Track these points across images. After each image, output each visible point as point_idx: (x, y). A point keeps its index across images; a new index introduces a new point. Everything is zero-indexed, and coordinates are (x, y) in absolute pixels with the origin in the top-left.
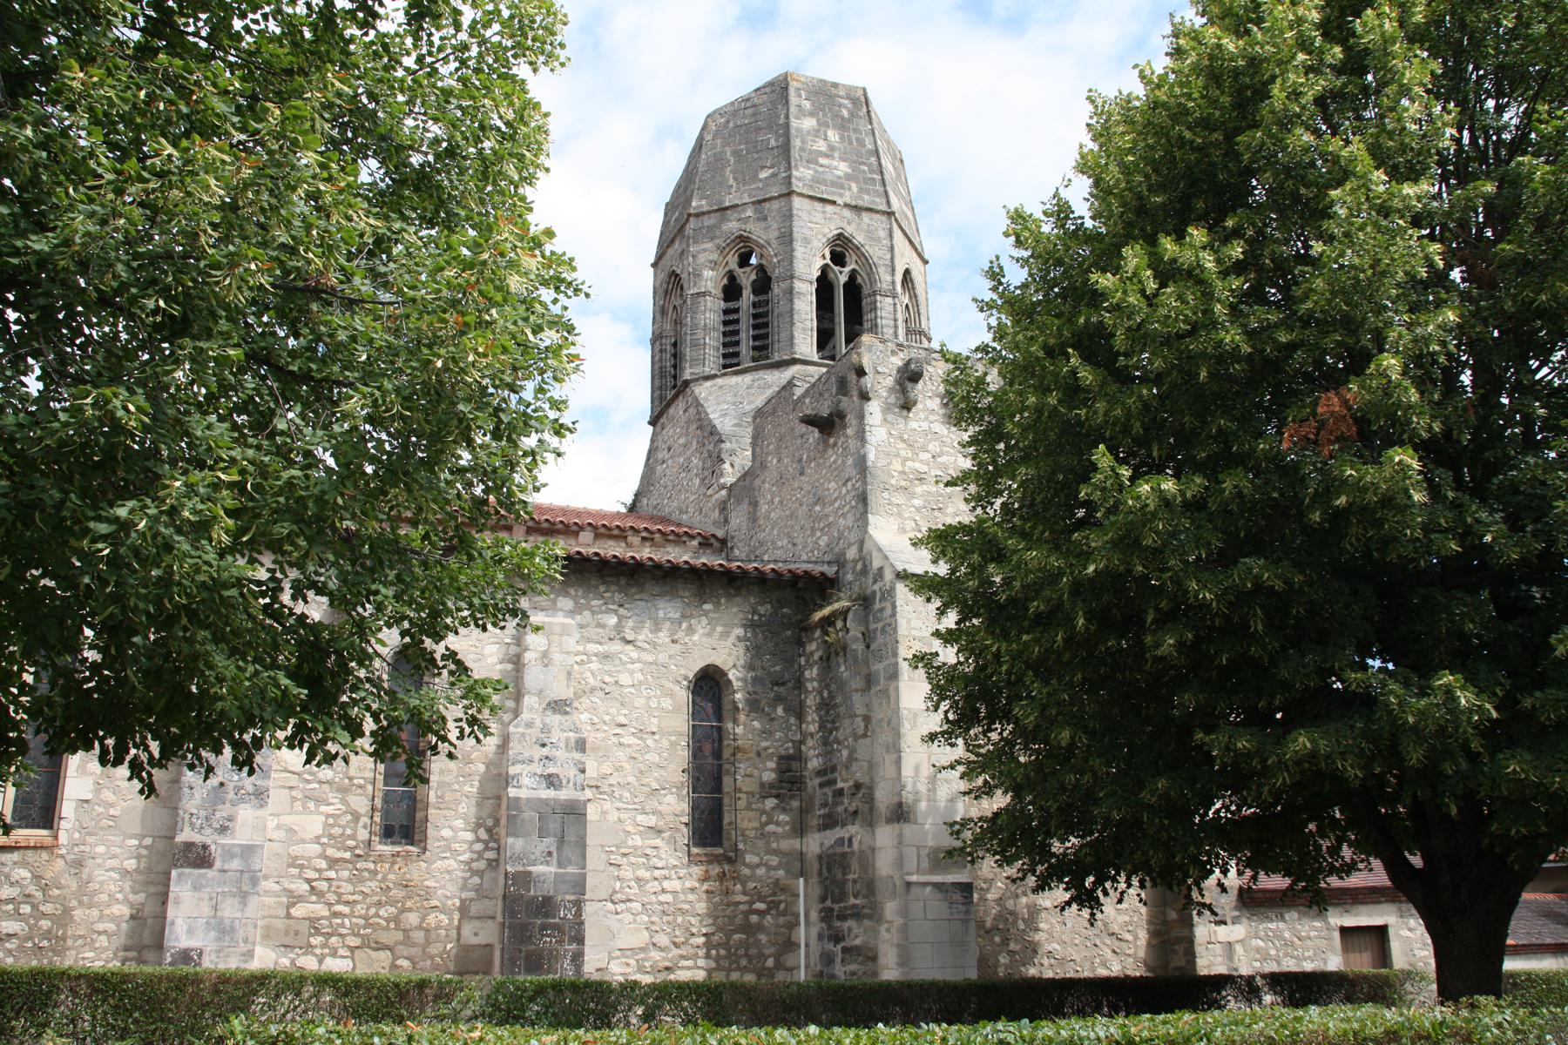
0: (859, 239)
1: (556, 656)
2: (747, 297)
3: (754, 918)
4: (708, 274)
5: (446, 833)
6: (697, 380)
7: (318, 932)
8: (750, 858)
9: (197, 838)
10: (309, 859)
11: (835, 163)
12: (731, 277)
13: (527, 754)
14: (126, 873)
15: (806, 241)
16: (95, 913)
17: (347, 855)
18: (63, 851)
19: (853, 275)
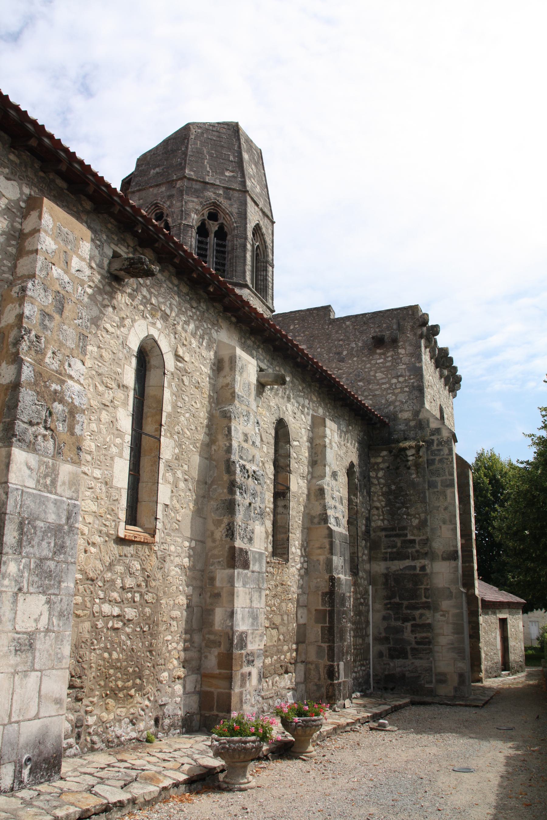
2: (212, 240)
14: (438, 652)
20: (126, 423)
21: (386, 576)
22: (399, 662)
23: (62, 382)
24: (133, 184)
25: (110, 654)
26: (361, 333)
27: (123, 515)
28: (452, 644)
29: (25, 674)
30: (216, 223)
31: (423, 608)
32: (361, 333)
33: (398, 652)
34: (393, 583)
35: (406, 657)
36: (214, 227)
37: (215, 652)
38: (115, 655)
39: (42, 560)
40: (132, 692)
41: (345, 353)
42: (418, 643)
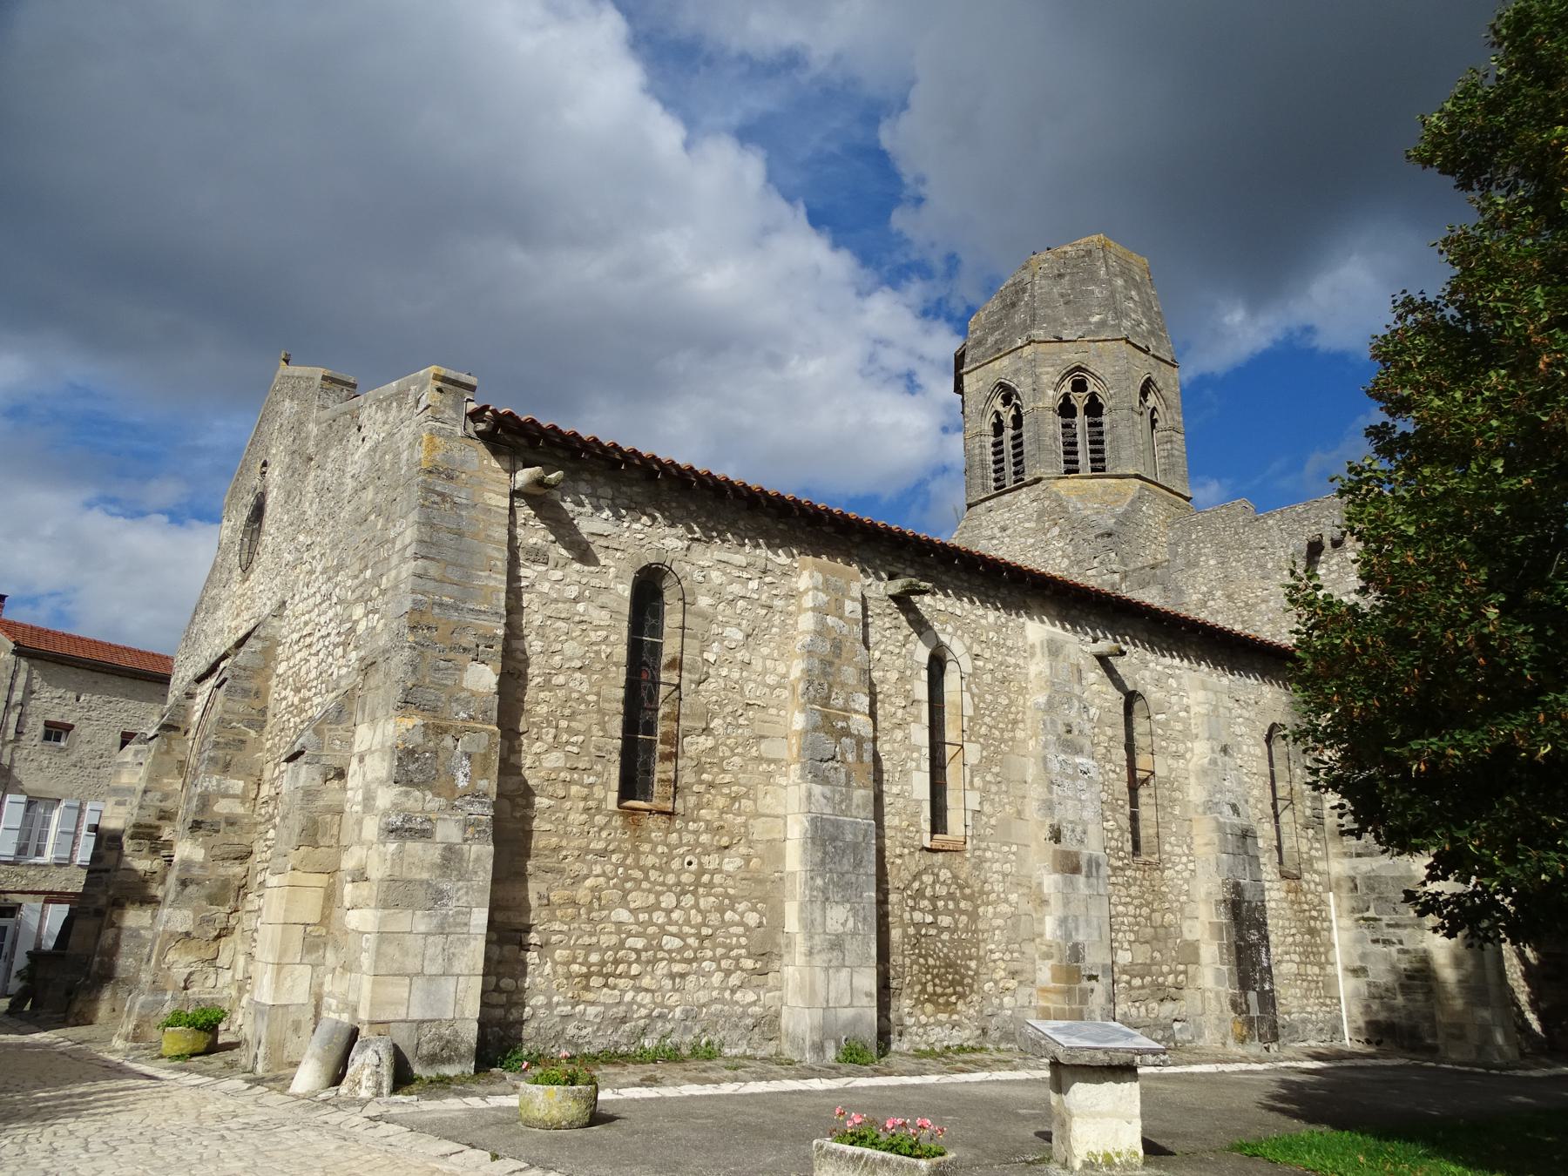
2: (1081, 420)
12: (1066, 397)
16: (990, 909)
23: (846, 719)
24: (967, 360)
26: (1291, 535)
27: (927, 826)
29: (838, 968)
32: (1291, 535)
36: (1080, 400)
40: (953, 999)
41: (1270, 565)
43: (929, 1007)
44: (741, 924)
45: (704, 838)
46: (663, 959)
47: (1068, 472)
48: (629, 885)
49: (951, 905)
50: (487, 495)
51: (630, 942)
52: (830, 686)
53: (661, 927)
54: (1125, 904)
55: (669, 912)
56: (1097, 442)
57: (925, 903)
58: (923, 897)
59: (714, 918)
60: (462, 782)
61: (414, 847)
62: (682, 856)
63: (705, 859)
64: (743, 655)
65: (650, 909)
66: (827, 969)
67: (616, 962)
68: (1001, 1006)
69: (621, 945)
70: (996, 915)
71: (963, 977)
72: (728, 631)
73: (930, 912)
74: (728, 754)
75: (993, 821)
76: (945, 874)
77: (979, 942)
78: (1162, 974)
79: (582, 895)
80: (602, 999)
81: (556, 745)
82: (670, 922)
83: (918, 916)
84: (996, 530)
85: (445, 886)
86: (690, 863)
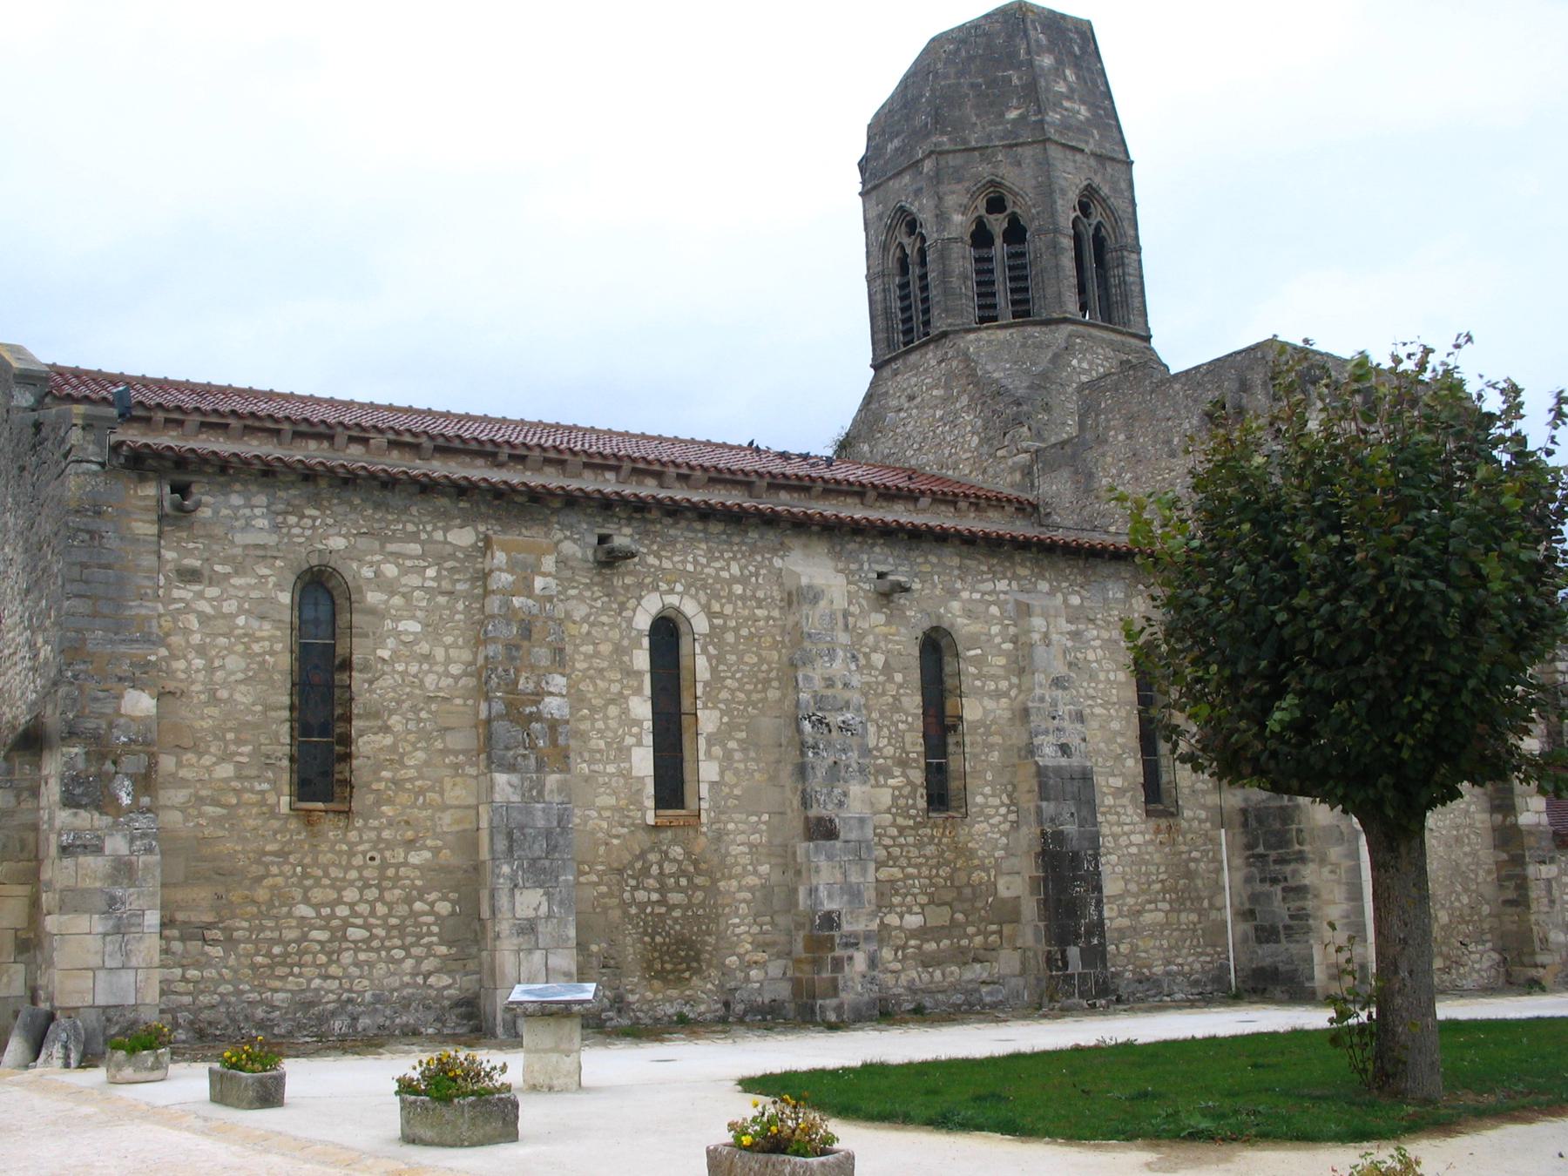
0: (1105, 190)
1: (1054, 637)
2: (999, 249)
3: (1192, 865)
4: (958, 218)
5: (979, 799)
6: (956, 332)
7: (897, 893)
8: (1187, 813)
9: (824, 813)
10: (884, 828)
11: (1077, 107)
12: (980, 223)
13: (1043, 727)
15: (1063, 192)
16: (734, 883)
17: (911, 823)
18: (704, 829)
19: (1099, 227)
20: (642, 708)
21: (1244, 812)
22: (1269, 948)
25: (653, 939)
28: (1347, 917)
29: (530, 951)
30: (1001, 216)
31: (1296, 860)
33: (1266, 934)
34: (1255, 824)
35: (1278, 941)
36: (997, 224)
37: (802, 933)
38: (659, 939)
39: (535, 860)
40: (687, 975)
42: (1292, 917)
43: (657, 984)
44: (432, 912)
45: (386, 834)
46: (348, 949)
47: (982, 320)
48: (308, 883)
49: (683, 882)
50: (134, 524)
51: (315, 934)
52: (517, 671)
53: (344, 919)
54: (917, 866)
55: (352, 905)
56: (1019, 275)
57: (651, 882)
58: (649, 876)
59: (402, 910)
60: (126, 800)
61: (89, 861)
62: (364, 853)
63: (388, 854)
64: (424, 648)
65: (333, 904)
66: (518, 951)
67: (301, 953)
68: (747, 979)
69: (304, 937)
70: (740, 889)
71: (699, 953)
72: (402, 626)
73: (656, 890)
74: (409, 748)
75: (737, 792)
76: (677, 851)
77: (718, 916)
78: (966, 936)
79: (262, 894)
80: (289, 986)
81: (225, 758)
82: (355, 914)
83: (641, 895)
84: (903, 399)
85: (119, 892)
86: (372, 859)
